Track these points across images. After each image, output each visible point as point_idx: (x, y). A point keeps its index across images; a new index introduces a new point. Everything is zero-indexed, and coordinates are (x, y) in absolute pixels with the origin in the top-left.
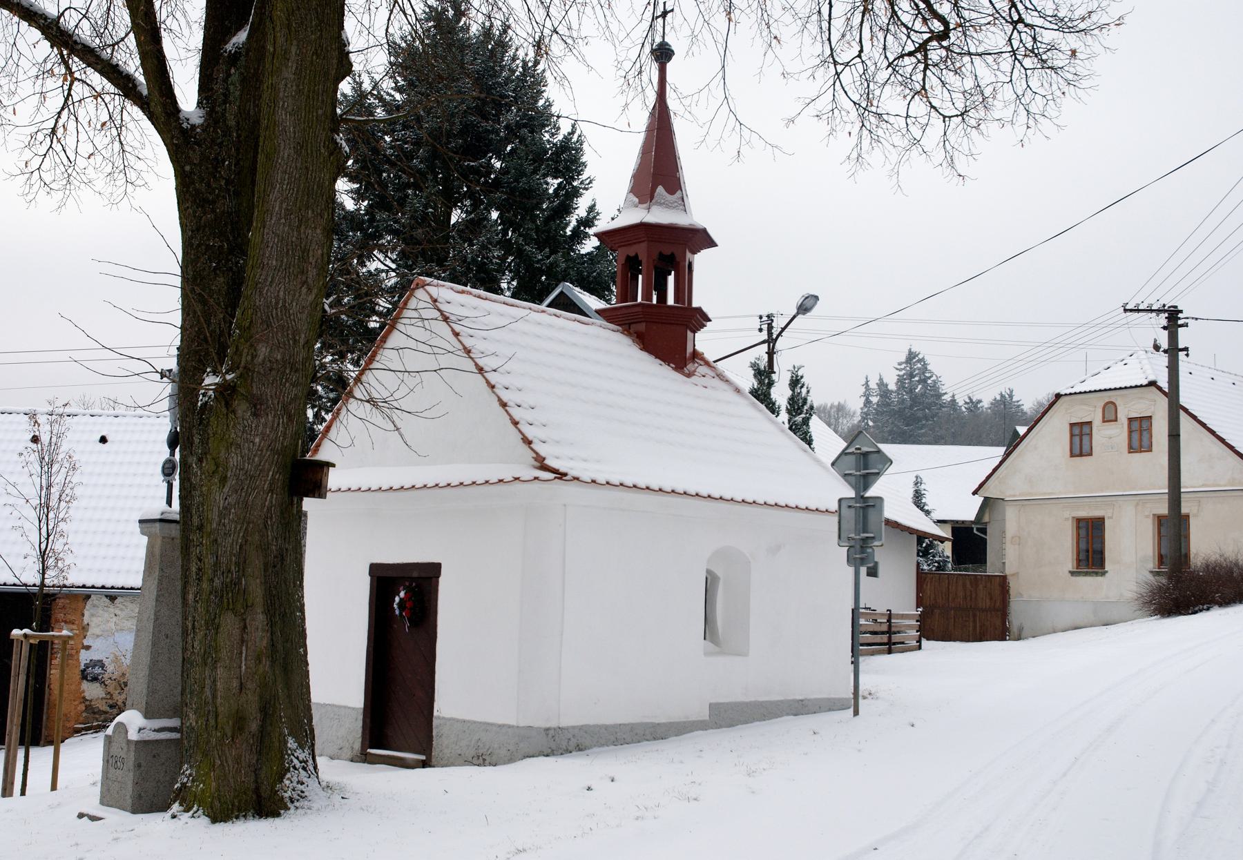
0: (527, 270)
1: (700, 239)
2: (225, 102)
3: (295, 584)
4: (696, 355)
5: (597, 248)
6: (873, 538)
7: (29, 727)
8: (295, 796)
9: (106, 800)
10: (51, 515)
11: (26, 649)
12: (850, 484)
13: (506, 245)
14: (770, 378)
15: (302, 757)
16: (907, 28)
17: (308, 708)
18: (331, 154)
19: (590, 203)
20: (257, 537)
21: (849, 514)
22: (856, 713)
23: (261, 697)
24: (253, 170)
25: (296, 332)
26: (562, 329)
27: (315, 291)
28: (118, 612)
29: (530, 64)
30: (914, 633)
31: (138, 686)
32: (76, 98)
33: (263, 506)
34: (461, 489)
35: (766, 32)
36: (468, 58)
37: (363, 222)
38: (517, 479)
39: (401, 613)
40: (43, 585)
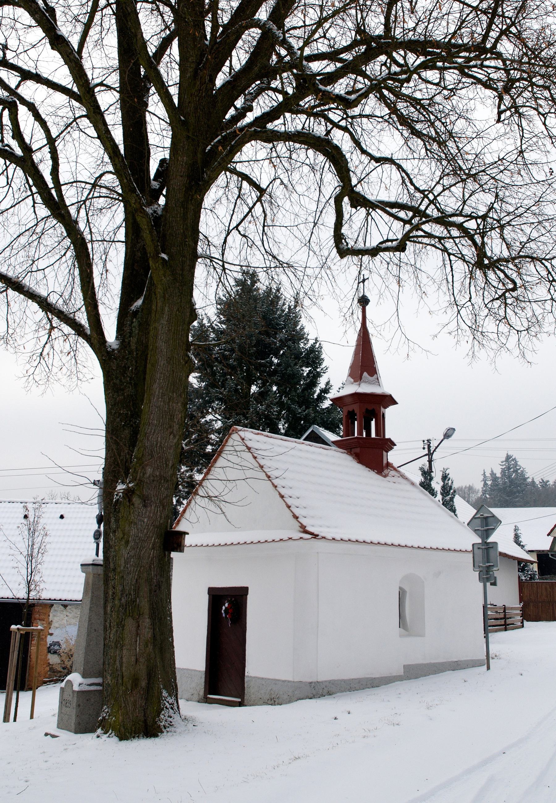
0: (293, 418)
1: (388, 400)
2: (130, 337)
3: (166, 601)
4: (389, 465)
5: (331, 405)
6: (493, 566)
7: (19, 682)
8: (167, 725)
9: (61, 725)
10: (34, 561)
11: (18, 636)
12: (478, 535)
13: (281, 405)
14: (430, 475)
15: (170, 701)
16: (494, 287)
17: (175, 668)
18: (186, 363)
19: (326, 381)
20: (145, 575)
21: (479, 553)
22: (488, 668)
23: (147, 667)
24: (145, 372)
25: (167, 460)
26: (314, 453)
27: (177, 437)
28: (68, 614)
29: (292, 307)
30: (519, 618)
31: (79, 659)
32: (53, 337)
33: (149, 557)
34: (259, 545)
35: (418, 291)
36: (259, 305)
37: (203, 394)
38: (290, 538)
39: (226, 616)
40: (28, 599)
